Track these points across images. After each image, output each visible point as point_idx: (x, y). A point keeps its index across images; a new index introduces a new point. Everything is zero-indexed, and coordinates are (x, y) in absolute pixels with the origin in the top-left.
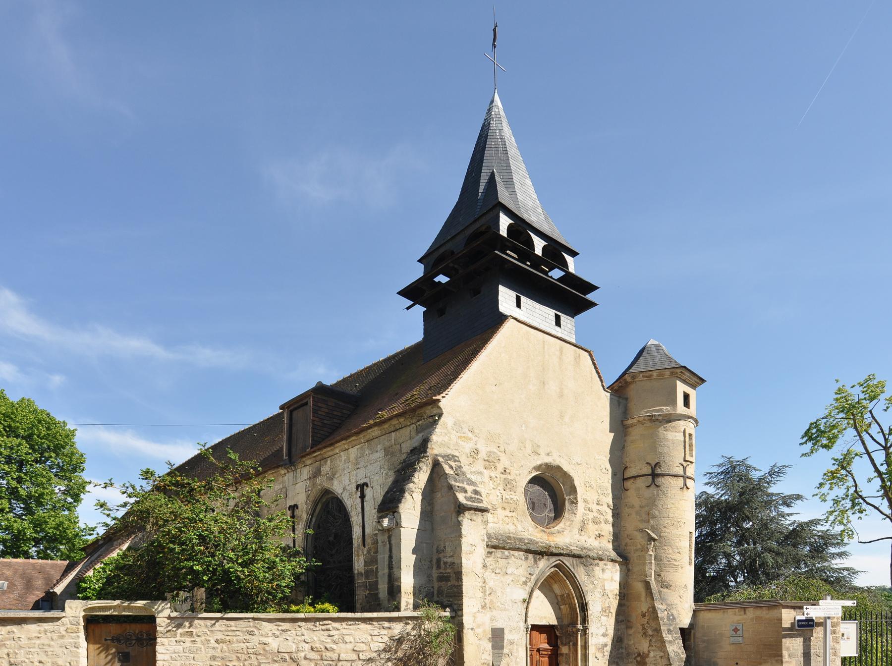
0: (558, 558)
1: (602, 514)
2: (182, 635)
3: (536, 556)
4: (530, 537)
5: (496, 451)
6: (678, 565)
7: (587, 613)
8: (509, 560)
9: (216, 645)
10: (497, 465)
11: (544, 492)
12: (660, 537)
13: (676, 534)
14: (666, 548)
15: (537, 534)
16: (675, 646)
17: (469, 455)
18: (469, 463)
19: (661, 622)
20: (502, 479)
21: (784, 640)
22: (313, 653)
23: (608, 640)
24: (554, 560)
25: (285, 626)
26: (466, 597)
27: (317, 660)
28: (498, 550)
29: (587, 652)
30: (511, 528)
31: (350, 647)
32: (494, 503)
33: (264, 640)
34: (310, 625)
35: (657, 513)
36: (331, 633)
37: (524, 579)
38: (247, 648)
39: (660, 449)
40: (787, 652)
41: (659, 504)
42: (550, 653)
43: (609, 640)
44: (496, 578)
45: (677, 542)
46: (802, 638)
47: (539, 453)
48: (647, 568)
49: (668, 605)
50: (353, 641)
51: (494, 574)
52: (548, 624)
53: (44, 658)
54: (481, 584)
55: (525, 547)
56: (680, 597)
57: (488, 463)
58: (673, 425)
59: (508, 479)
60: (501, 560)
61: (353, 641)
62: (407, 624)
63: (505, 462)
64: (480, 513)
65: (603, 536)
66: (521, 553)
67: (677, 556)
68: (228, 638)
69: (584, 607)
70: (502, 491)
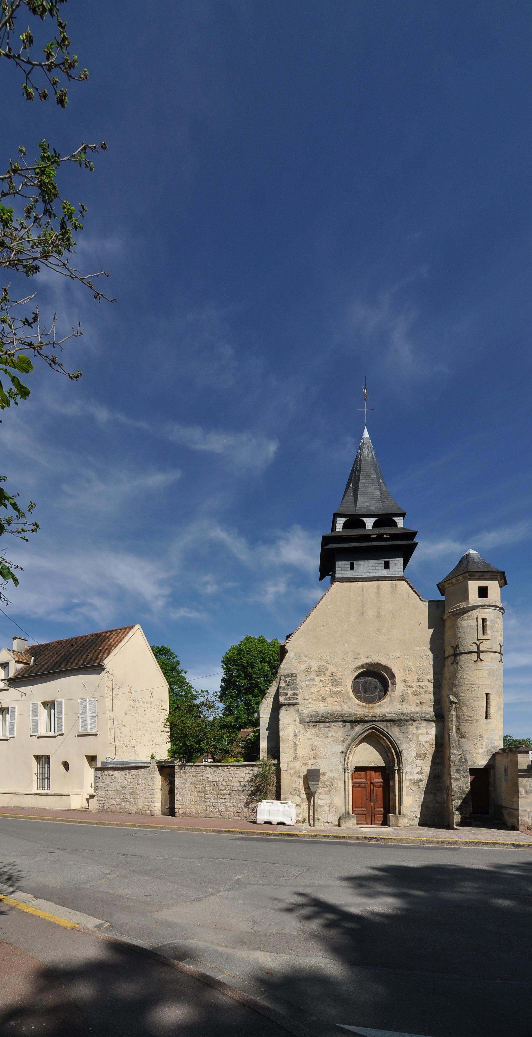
1: (422, 688)
2: (182, 773)
3: (353, 724)
5: (325, 664)
6: (473, 720)
7: (401, 759)
9: (193, 778)
10: (325, 672)
11: (375, 680)
12: (459, 700)
13: (471, 697)
14: (463, 708)
15: (359, 709)
16: (461, 782)
17: (304, 671)
19: (452, 764)
21: (520, 779)
22: (224, 782)
25: (215, 769)
26: (282, 753)
27: (225, 785)
28: (321, 723)
29: (402, 785)
30: (339, 708)
31: (237, 779)
33: (208, 776)
34: (223, 768)
35: (457, 683)
36: (231, 772)
37: (342, 739)
38: (202, 779)
39: (459, 635)
40: (523, 789)
41: (458, 675)
42: (382, 785)
43: (425, 778)
44: (320, 740)
45: (472, 703)
46: (519, 779)
48: (450, 724)
49: (464, 751)
50: (238, 776)
51: (317, 738)
52: (376, 766)
53: (146, 783)
54: (293, 745)
56: (474, 745)
58: (468, 615)
61: (238, 776)
62: (260, 768)
63: (332, 669)
64: (292, 706)
65: (424, 703)
66: (340, 723)
67: (472, 714)
68: (196, 774)
69: (399, 754)
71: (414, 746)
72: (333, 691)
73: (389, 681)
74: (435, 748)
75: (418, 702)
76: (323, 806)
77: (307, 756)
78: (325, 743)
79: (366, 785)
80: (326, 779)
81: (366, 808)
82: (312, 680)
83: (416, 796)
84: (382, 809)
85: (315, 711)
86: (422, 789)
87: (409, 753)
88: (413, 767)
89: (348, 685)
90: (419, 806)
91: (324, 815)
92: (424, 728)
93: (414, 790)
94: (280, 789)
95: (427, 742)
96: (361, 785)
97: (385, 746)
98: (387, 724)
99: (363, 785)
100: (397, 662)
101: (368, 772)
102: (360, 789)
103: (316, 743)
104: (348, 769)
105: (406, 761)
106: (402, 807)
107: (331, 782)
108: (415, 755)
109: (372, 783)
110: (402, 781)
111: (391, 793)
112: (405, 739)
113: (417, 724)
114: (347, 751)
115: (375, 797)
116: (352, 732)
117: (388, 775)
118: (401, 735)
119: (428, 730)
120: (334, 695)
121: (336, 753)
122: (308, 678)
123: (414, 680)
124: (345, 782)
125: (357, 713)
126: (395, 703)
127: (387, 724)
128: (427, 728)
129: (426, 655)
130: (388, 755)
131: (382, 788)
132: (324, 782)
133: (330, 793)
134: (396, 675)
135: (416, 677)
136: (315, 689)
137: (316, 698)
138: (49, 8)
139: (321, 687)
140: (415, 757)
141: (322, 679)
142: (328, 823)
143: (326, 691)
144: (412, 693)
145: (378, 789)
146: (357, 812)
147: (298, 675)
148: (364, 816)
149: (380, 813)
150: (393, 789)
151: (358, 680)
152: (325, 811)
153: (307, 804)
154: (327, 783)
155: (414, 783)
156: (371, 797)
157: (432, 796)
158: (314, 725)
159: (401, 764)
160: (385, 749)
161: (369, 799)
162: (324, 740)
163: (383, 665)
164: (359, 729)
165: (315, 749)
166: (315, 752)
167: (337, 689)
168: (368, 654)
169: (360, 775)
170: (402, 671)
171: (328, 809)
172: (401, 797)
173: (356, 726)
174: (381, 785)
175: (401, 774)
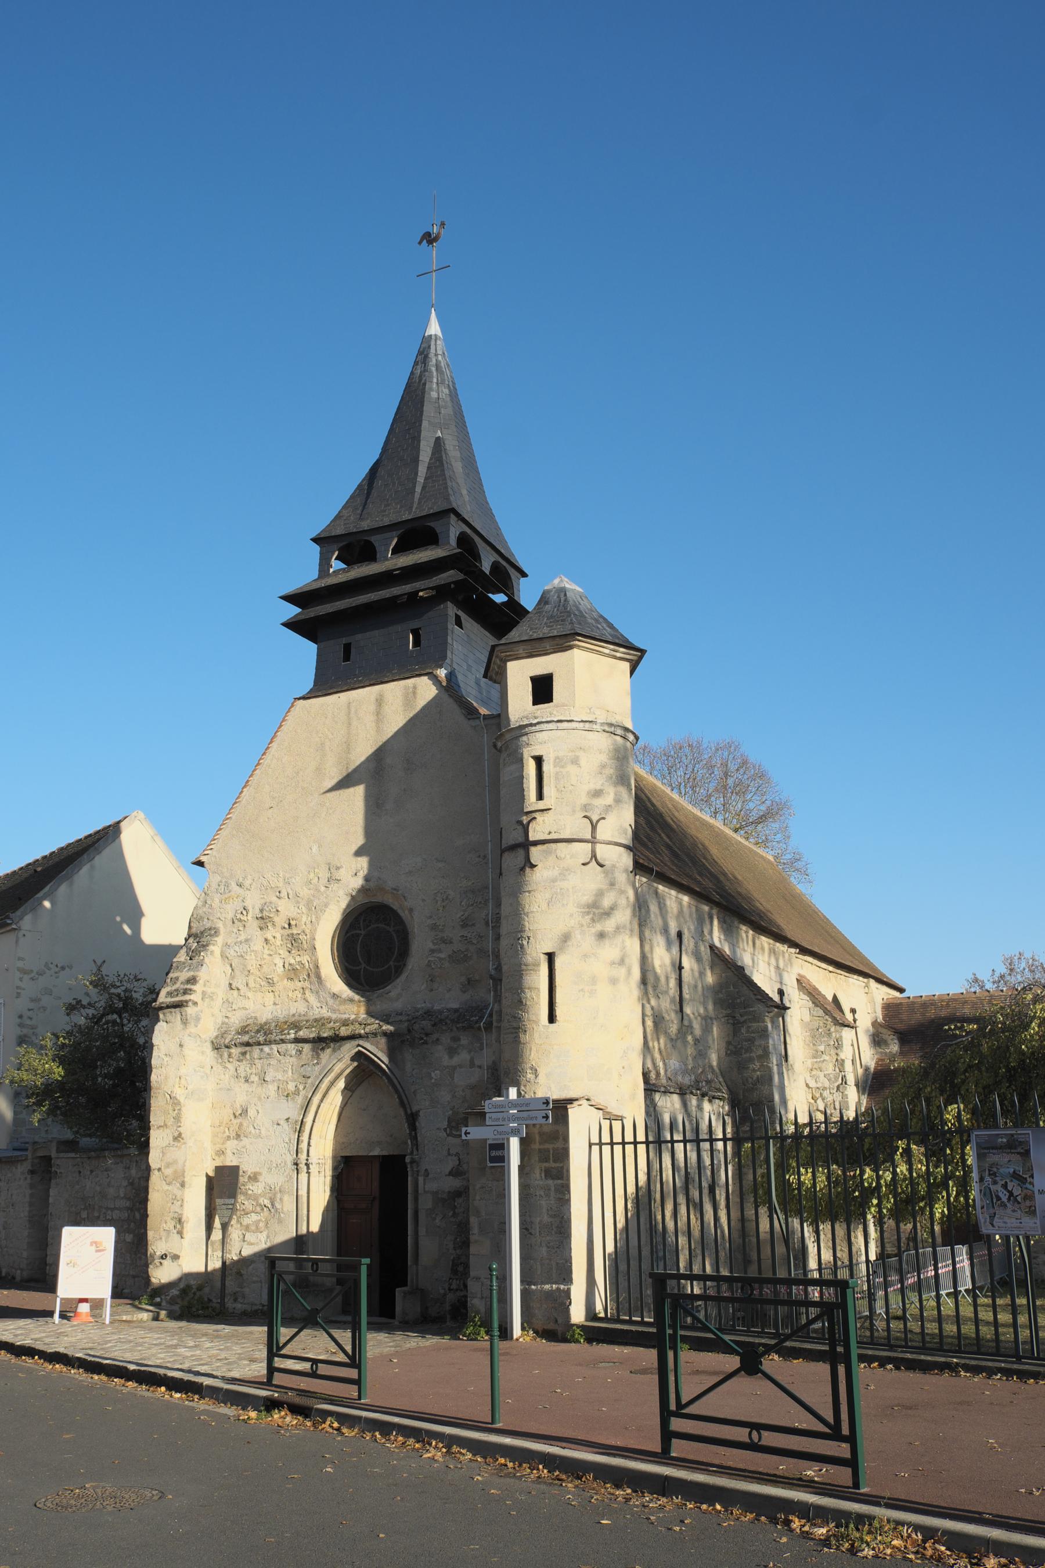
0: (357, 1042)
24: (349, 1049)
26: (154, 1126)
32: (270, 977)
47: (339, 878)
57: (262, 921)
94: (147, 1216)
119: (472, 1053)
128: (470, 1052)
132: (256, 1198)
135: (459, 915)
140: (445, 1130)
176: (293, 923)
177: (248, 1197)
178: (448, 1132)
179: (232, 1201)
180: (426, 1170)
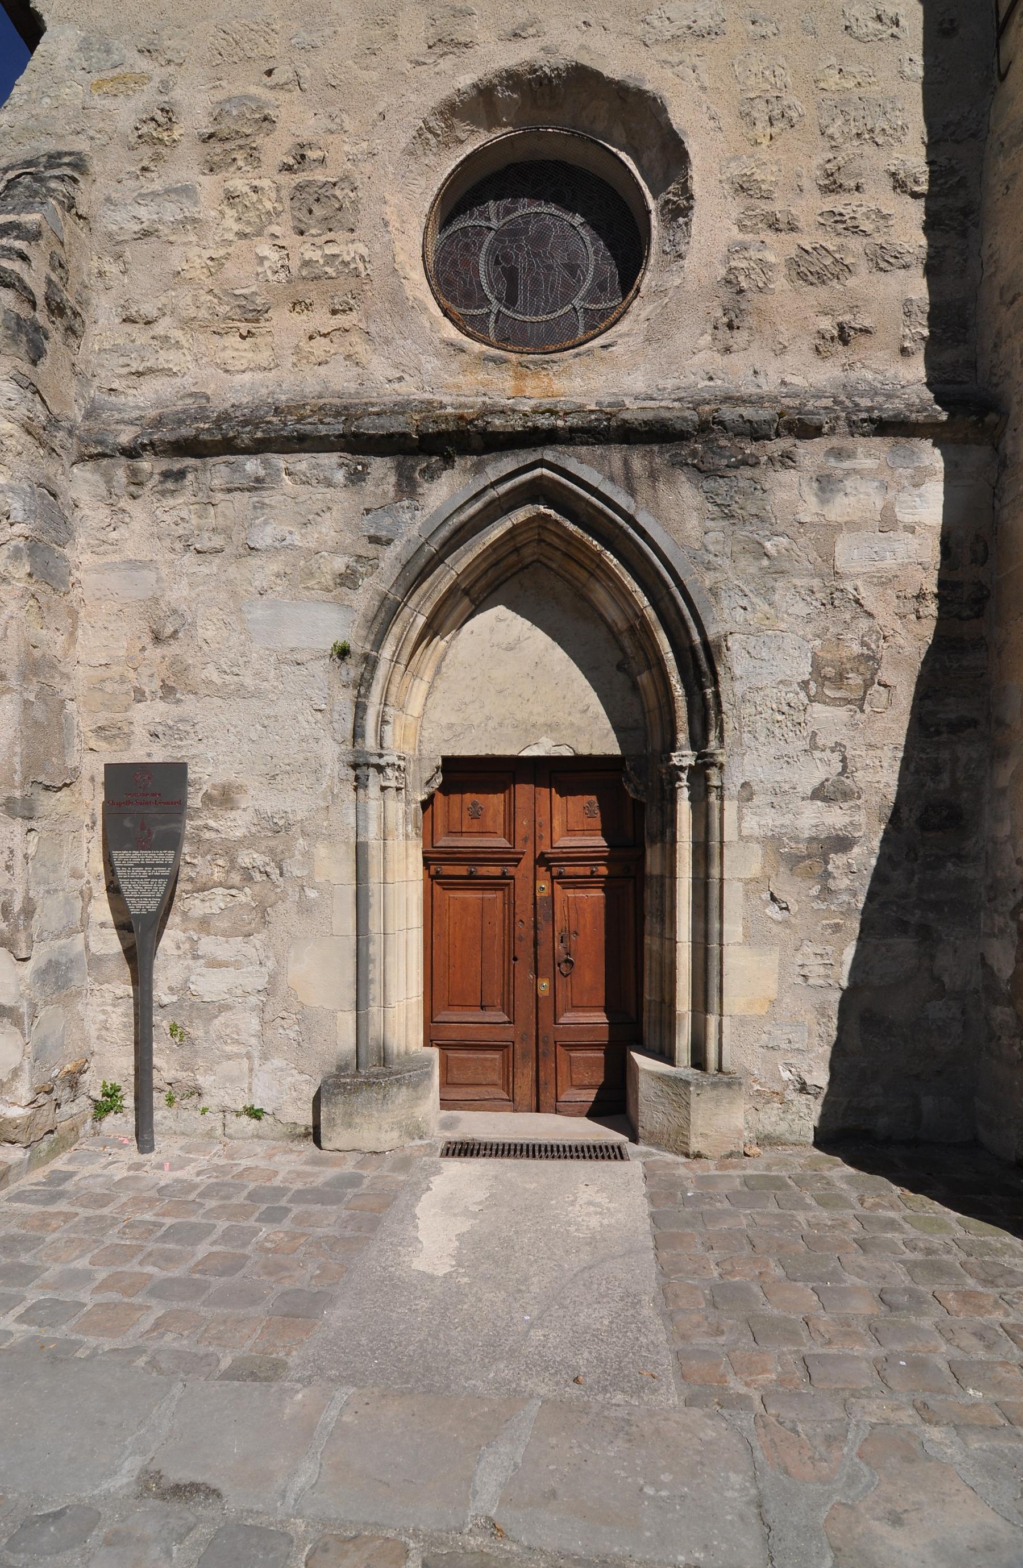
1: (856, 230)
3: (410, 461)
4: (427, 396)
5: (253, 90)
7: (717, 695)
8: (264, 493)
10: (259, 141)
11: (568, 217)
15: (461, 379)
17: (133, 139)
18: (136, 169)
20: (285, 193)
23: (861, 818)
28: (211, 461)
29: (715, 872)
37: (339, 564)
42: (603, 870)
44: (205, 570)
51: (190, 558)
52: (567, 752)
55: (339, 428)
59: (310, 183)
60: (228, 496)
65: (865, 331)
66: (330, 460)
70: (291, 240)
71: (801, 609)
72: (306, 263)
73: (652, 204)
74: (939, 620)
75: (827, 324)
76: (224, 1008)
77: (123, 680)
78: (234, 595)
79: (511, 871)
80: (239, 833)
81: (509, 1007)
82: (175, 191)
83: (808, 949)
84: (600, 1018)
85: (191, 395)
86: (845, 897)
87: (764, 654)
88: (789, 750)
89: (395, 223)
90: (822, 1011)
91: (228, 1067)
92: (870, 487)
93: (794, 908)
95: (884, 581)
96: (483, 871)
97: (621, 624)
98: (626, 464)
99: (495, 871)
100: (696, 61)
101: (524, 791)
102: (479, 895)
103: (178, 594)
104: (380, 769)
105: (748, 710)
106: (713, 1020)
107: (271, 852)
108: (805, 670)
109: (542, 860)
110: (715, 844)
111: (651, 924)
112: (743, 562)
113: (820, 459)
114: (378, 644)
115: (559, 947)
116: (408, 516)
117: (639, 807)
118: (717, 535)
120: (311, 292)
121: (299, 657)
122: (157, 186)
123: (806, 183)
124: (360, 851)
125: (446, 399)
126: (682, 339)
127: (626, 464)
128: (885, 487)
129: (879, 18)
130: (635, 687)
131: (604, 889)
132: (229, 850)
133: (266, 923)
134: (692, 146)
136: (193, 252)
137: (203, 313)
138: (629, 780)
139: (230, 236)
140: (804, 685)
141: (239, 184)
142: (255, 1114)
143: (261, 260)
144: (793, 264)
145: (580, 894)
146: (453, 1034)
147: (95, 166)
148: (497, 1056)
149: (586, 1039)
150: (662, 898)
151: (471, 223)
152: (237, 1042)
153: (130, 990)
154: (245, 858)
155: (793, 861)
156: (536, 944)
157: (905, 945)
158: (166, 475)
159: (713, 735)
160: (622, 649)
161: (526, 951)
162: (232, 571)
163: (611, 81)
164: (453, 495)
165: (175, 634)
166: (173, 649)
167: (330, 250)
168: (522, 15)
169: (476, 814)
170: (728, 121)
171: (255, 1024)
172: (707, 951)
173: (431, 474)
174: (592, 875)
175: (713, 797)
176: (312, 154)
177: (206, 847)
178: (812, 692)
179: (171, 854)
180: (745, 785)
